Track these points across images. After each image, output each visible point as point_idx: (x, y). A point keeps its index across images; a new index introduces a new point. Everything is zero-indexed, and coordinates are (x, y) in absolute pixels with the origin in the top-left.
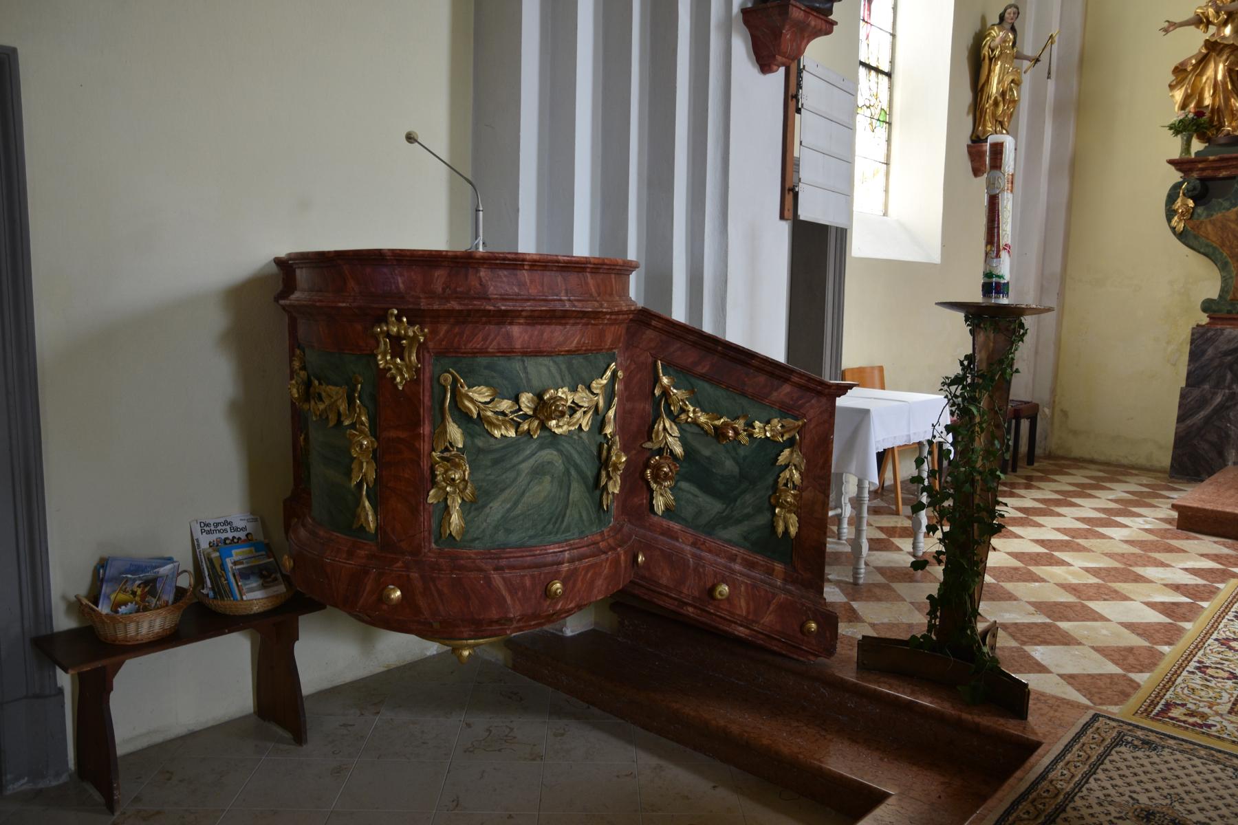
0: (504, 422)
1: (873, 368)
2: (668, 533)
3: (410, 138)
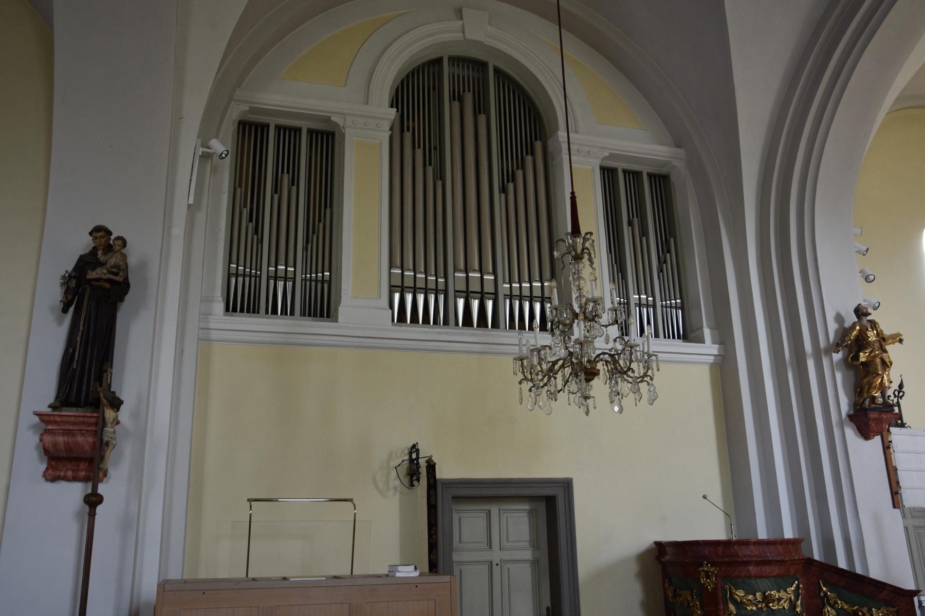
0: (751, 604)
3: (704, 497)
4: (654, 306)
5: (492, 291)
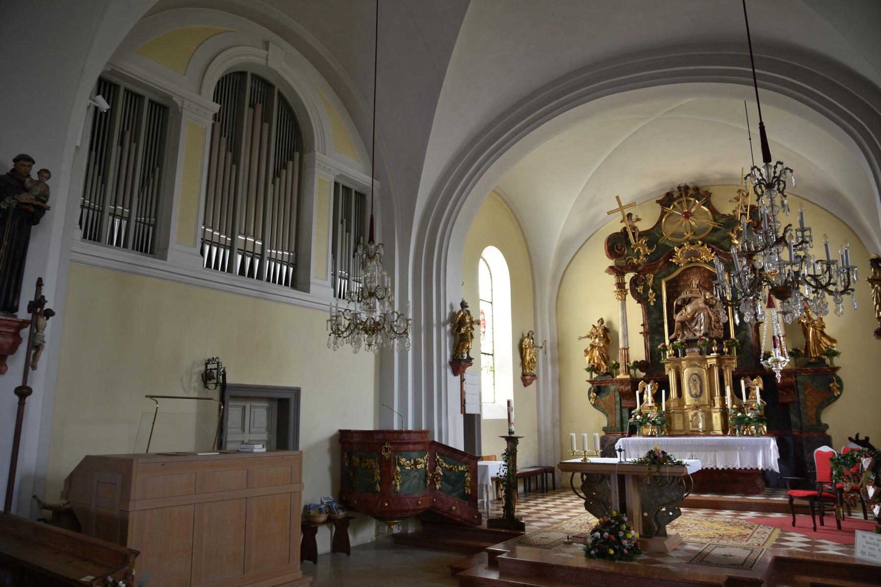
1: (492, 456)
2: (440, 494)
4: (129, 220)
5: (127, 216)
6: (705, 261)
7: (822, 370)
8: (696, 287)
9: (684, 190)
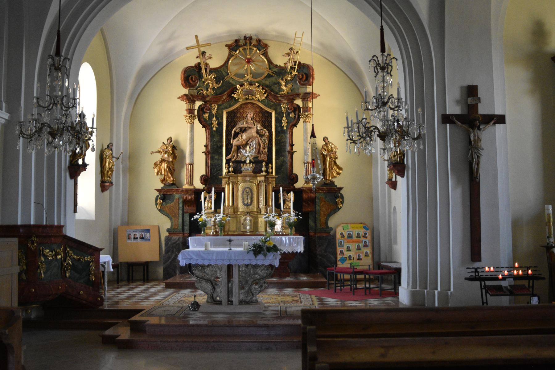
6: (258, 99)
7: (332, 189)
8: (251, 119)
9: (248, 40)
